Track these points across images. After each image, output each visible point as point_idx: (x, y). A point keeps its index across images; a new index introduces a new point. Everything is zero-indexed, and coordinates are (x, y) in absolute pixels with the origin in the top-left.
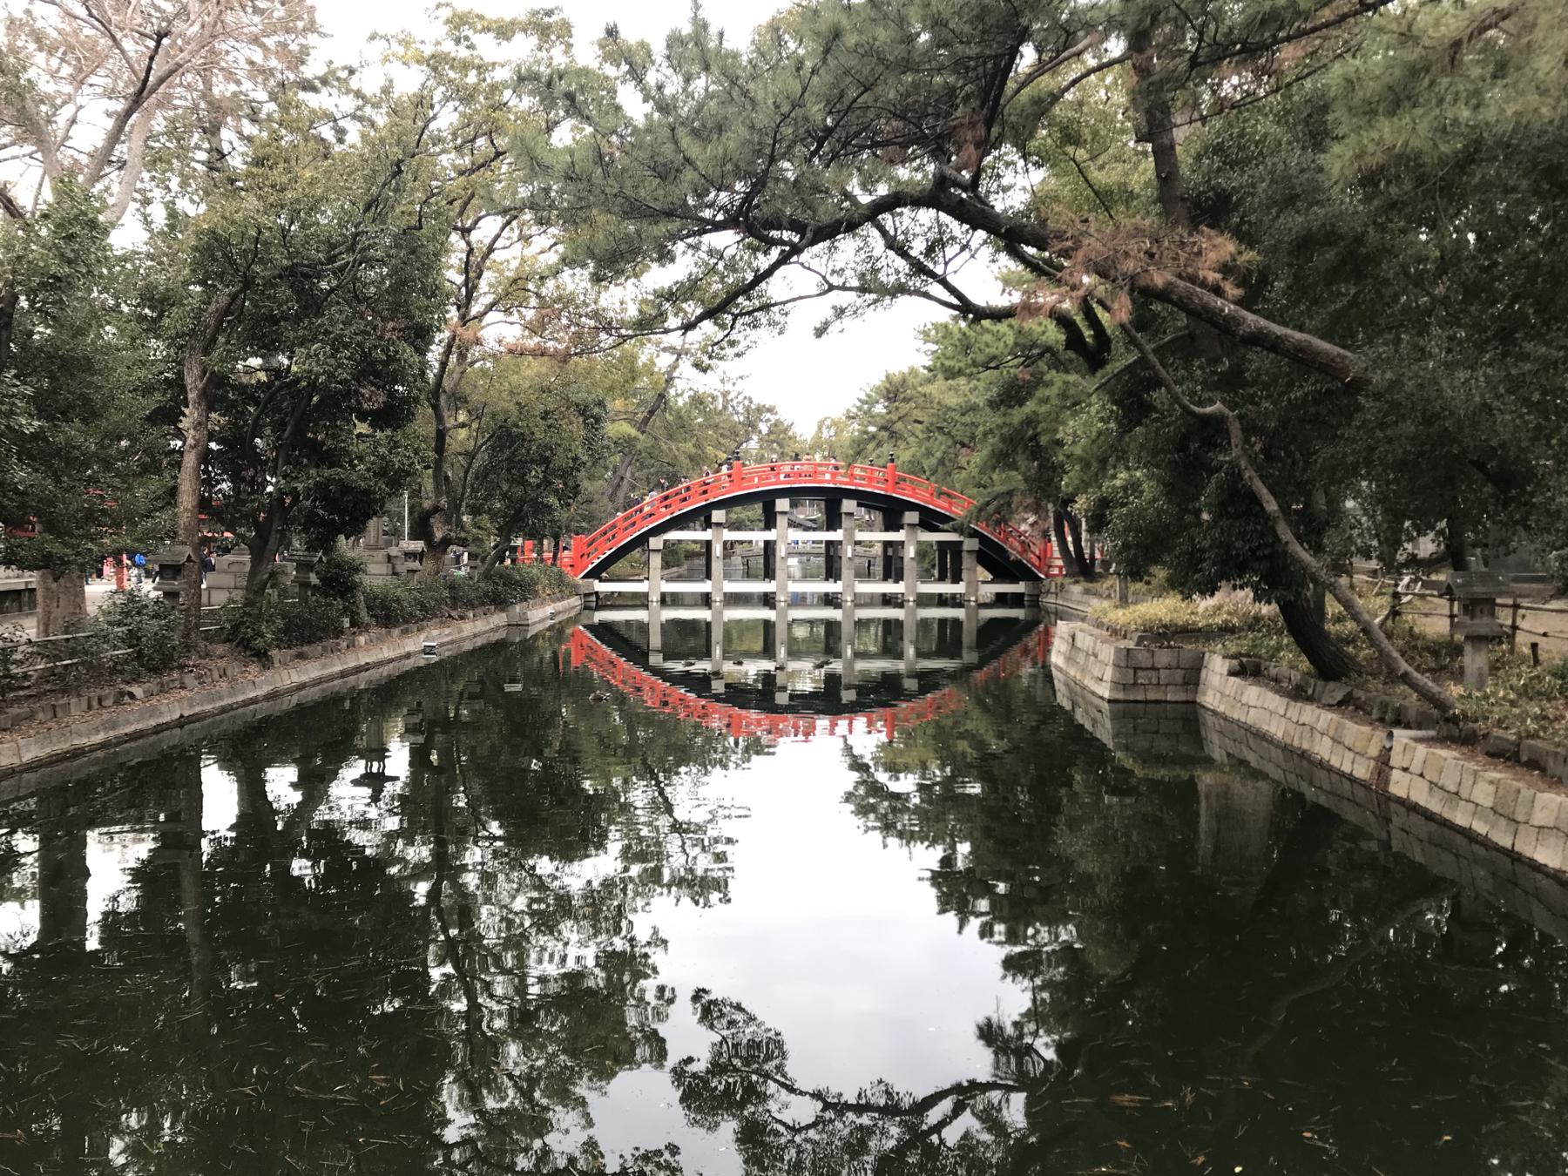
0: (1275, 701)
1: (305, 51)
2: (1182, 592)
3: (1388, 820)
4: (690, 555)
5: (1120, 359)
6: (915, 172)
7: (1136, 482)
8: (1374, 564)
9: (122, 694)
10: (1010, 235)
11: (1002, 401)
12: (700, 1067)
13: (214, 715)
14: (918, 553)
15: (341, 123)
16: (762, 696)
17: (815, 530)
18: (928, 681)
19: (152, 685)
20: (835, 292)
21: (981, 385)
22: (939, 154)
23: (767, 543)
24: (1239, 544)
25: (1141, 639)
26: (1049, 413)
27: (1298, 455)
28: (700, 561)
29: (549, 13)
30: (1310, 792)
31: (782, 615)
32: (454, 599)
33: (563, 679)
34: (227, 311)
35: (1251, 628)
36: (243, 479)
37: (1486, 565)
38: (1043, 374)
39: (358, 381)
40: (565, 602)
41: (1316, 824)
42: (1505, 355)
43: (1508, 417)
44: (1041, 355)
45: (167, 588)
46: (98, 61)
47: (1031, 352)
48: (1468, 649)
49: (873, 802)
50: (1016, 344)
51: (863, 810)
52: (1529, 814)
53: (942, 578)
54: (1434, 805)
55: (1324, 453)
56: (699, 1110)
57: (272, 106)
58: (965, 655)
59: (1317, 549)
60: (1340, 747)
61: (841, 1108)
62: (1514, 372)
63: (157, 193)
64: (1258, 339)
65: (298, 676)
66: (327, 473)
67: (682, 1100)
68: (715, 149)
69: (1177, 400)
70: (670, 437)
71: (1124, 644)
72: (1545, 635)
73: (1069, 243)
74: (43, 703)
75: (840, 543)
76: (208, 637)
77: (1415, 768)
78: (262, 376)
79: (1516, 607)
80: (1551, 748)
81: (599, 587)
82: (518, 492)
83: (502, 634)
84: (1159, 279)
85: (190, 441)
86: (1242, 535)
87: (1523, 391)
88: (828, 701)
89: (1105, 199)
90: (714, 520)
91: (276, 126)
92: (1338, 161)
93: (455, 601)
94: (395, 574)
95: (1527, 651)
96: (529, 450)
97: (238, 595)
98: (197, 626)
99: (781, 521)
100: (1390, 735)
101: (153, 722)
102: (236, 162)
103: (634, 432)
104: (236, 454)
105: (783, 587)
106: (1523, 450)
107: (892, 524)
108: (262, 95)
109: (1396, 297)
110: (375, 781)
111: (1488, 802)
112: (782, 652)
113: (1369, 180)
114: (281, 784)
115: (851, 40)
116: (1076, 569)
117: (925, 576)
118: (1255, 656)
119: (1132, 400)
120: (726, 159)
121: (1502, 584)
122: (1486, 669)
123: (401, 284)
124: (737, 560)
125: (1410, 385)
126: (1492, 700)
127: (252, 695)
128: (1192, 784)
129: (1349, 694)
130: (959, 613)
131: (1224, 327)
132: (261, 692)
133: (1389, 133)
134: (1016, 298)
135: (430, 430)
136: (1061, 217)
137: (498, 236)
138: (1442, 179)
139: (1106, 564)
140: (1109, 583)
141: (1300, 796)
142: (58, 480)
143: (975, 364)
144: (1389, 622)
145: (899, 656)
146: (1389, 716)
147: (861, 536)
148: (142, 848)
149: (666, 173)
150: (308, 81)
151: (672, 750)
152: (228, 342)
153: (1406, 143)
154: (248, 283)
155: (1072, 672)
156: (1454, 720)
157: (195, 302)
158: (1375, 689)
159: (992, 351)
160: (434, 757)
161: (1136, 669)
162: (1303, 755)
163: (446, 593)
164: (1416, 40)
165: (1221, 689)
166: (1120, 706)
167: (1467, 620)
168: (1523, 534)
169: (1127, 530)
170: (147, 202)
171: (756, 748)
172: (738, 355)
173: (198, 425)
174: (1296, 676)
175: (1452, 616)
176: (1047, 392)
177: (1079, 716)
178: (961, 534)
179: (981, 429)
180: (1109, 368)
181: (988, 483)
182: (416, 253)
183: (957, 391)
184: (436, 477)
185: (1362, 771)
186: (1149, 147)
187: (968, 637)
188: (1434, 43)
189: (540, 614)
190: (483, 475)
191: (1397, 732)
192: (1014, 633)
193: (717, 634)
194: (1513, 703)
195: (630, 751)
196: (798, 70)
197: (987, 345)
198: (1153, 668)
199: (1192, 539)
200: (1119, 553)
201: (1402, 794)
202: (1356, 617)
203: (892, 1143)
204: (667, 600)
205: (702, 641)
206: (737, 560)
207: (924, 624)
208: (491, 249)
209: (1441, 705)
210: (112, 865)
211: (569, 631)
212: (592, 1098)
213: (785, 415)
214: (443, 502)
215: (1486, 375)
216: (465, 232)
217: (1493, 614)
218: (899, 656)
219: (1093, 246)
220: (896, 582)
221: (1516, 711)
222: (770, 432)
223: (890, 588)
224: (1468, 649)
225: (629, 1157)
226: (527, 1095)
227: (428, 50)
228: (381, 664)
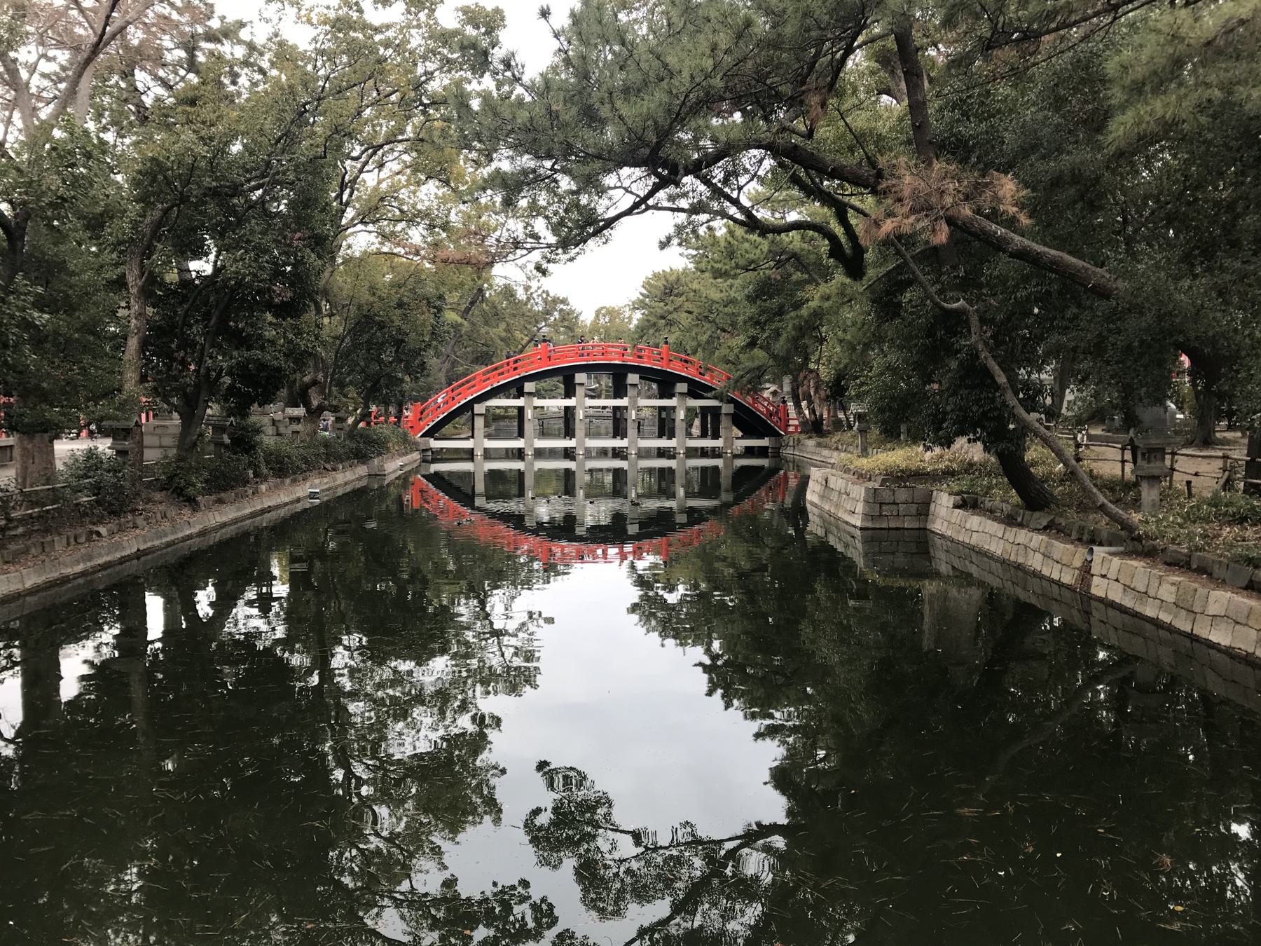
9: (91, 532)
11: (757, 296)
13: (161, 549)
16: (564, 529)
18: (695, 516)
20: (650, 211)
24: (975, 409)
25: (883, 482)
33: (403, 517)
34: (158, 224)
35: (967, 471)
36: (175, 360)
40: (409, 456)
44: (788, 260)
45: (120, 447)
49: (650, 609)
50: (770, 251)
51: (647, 617)
54: (1128, 602)
60: (1050, 561)
65: (218, 517)
67: (531, 842)
70: (486, 323)
71: (871, 485)
72: (1196, 474)
75: (626, 408)
77: (1112, 575)
80: (1216, 558)
81: (435, 444)
83: (363, 483)
86: (977, 401)
88: (611, 533)
90: (526, 390)
94: (279, 434)
98: (140, 477)
99: (580, 391)
101: (118, 555)
103: (459, 320)
105: (581, 443)
107: (666, 392)
110: (264, 603)
111: (1171, 599)
121: (1170, 437)
127: (188, 532)
128: (915, 595)
130: (719, 462)
132: (194, 530)
143: (737, 266)
145: (672, 496)
151: (497, 570)
154: (184, 199)
155: (827, 507)
156: (1139, 539)
158: (1071, 517)
159: (751, 256)
162: (1019, 567)
163: (322, 450)
165: (946, 516)
166: (870, 532)
171: (551, 569)
174: (1007, 508)
178: (721, 401)
181: (741, 358)
185: (1068, 578)
187: (725, 480)
189: (393, 466)
191: (1095, 548)
194: (1181, 526)
197: (747, 252)
198: (894, 503)
204: (488, 454)
209: (1128, 527)
211: (411, 480)
212: (446, 846)
213: (576, 304)
218: (672, 496)
220: (670, 438)
223: (664, 443)
228: (279, 507)
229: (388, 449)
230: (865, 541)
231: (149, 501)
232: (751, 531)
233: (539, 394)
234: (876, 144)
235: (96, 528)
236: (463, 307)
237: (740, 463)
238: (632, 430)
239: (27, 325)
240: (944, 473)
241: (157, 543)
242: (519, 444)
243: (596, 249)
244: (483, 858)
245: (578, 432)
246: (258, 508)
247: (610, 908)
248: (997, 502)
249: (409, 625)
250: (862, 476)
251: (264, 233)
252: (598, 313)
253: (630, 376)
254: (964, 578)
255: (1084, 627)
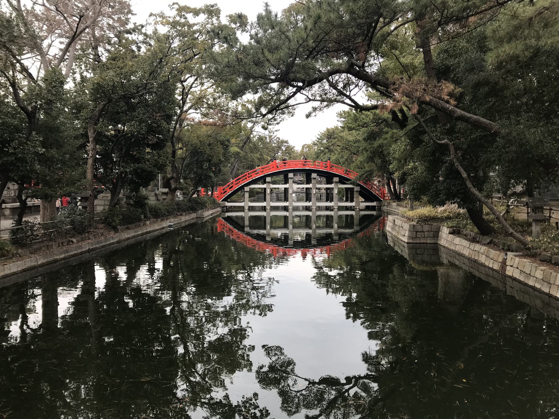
0: (465, 243)
1: (128, 20)
2: (433, 205)
3: (505, 284)
4: (258, 193)
5: (412, 124)
6: (341, 61)
7: (417, 167)
8: (499, 195)
9: (69, 241)
10: (373, 82)
11: (368, 139)
12: (265, 369)
14: (338, 192)
15: (139, 44)
16: (284, 241)
17: (301, 184)
18: (341, 236)
19: (79, 238)
21: (361, 133)
22: (348, 53)
23: (285, 189)
24: (453, 188)
25: (418, 222)
26: (387, 143)
27: (474, 157)
28: (260, 195)
29: (212, 6)
30: (477, 274)
31: (291, 214)
32: (178, 209)
34: (102, 110)
35: (457, 217)
37: (540, 195)
38: (383, 129)
39: (147, 134)
41: (479, 287)
42: (547, 123)
43: (548, 145)
44: (382, 122)
46: (59, 24)
47: (378, 121)
48: (534, 224)
49: (323, 280)
50: (373, 118)
52: (555, 281)
53: (347, 201)
54: (522, 278)
55: (484, 157)
56: (264, 384)
57: (116, 39)
58: (355, 227)
59: (480, 190)
60: (489, 259)
61: (314, 383)
62: (551, 129)
63: (77, 70)
64: (461, 118)
66: (137, 165)
68: (276, 56)
69: (431, 138)
70: (252, 152)
73: (397, 86)
74: (44, 244)
75: (311, 188)
76: (98, 222)
77: (515, 266)
78: (113, 132)
79: (551, 209)
81: (227, 204)
82: (200, 171)
84: (428, 99)
85: (90, 155)
86: (454, 185)
87: (554, 135)
88: (305, 245)
89: (405, 68)
90: (267, 181)
91: (117, 46)
92: (490, 59)
93: (179, 209)
95: (554, 225)
96: (203, 157)
97: (107, 207)
98: (93, 218)
99: (290, 181)
100: (506, 254)
101: (80, 251)
102: (104, 59)
103: (239, 150)
104: (105, 160)
106: (553, 156)
107: (329, 182)
108: (112, 35)
109: (509, 103)
111: (540, 277)
112: (291, 226)
113: (499, 66)
114: (122, 272)
115: (324, 19)
116: (394, 197)
117: (341, 200)
118: (458, 227)
119: (416, 139)
120: (280, 59)
121: (545, 202)
122: (540, 231)
123: (161, 98)
124: (274, 195)
125: (514, 134)
126: (542, 242)
127: (112, 242)
128: (435, 272)
129: (491, 240)
130: (353, 213)
131: (449, 115)
133: (508, 49)
134: (374, 102)
135: (170, 150)
136: (392, 77)
137: (193, 83)
138: (526, 62)
139: (405, 196)
140: (406, 202)
141: (474, 277)
142: (49, 169)
143: (359, 125)
144: (506, 215)
145: (332, 227)
146: (506, 248)
147: (318, 186)
148: (76, 293)
149: (258, 63)
150: (128, 30)
151: (259, 260)
152: (103, 121)
153: (514, 53)
154: (110, 101)
156: (529, 249)
157: (91, 107)
159: (365, 121)
160: (172, 263)
161: (416, 232)
162: (476, 261)
163: (176, 207)
164: (517, 18)
165: (446, 238)
167: (533, 214)
168: (553, 184)
169: (414, 184)
170: (74, 73)
172: (278, 124)
173: (93, 149)
174: (473, 234)
175: (528, 213)
176: (386, 136)
177: (396, 248)
179: (361, 148)
180: (408, 127)
181: (362, 164)
182: (167, 89)
183: (352, 135)
184: (172, 167)
185: (496, 267)
186: (421, 50)
187: (356, 221)
188: (523, 18)
189: (208, 214)
190: (188, 166)
191: (508, 253)
192: (373, 220)
193: (268, 221)
194: (549, 243)
195: (237, 262)
196: (305, 29)
197: (363, 119)
199: (436, 187)
200: (411, 191)
201: (510, 274)
202: (494, 214)
203: (332, 397)
204: (251, 209)
205: (263, 223)
206: (274, 195)
207: (340, 217)
208: (191, 87)
209: (524, 244)
210: (65, 301)
213: (291, 143)
214: (175, 175)
215: (541, 130)
216: (182, 82)
217: (542, 212)
218: (332, 227)
219: (405, 86)
220: (331, 202)
221: (550, 246)
222: (286, 150)
223: (328, 204)
224: (534, 224)
225: (240, 402)
226: (203, 379)
227: (171, 20)
229: (206, 207)
230: (409, 249)
231: (97, 228)
232: (367, 243)
233: (274, 183)
234: (413, 70)
235: (71, 239)
236: (241, 145)
237: (363, 213)
238: (313, 199)
239: (36, 153)
240: (446, 218)
241: (98, 246)
242: (264, 204)
243: (288, 119)
244: (239, 386)
245: (313, 199)
246: (145, 231)
247: (293, 410)
248: (468, 232)
249: (213, 284)
250: (409, 219)
251: (144, 114)
252: (303, 147)
253: (313, 174)
254: (452, 265)
255: (504, 289)
